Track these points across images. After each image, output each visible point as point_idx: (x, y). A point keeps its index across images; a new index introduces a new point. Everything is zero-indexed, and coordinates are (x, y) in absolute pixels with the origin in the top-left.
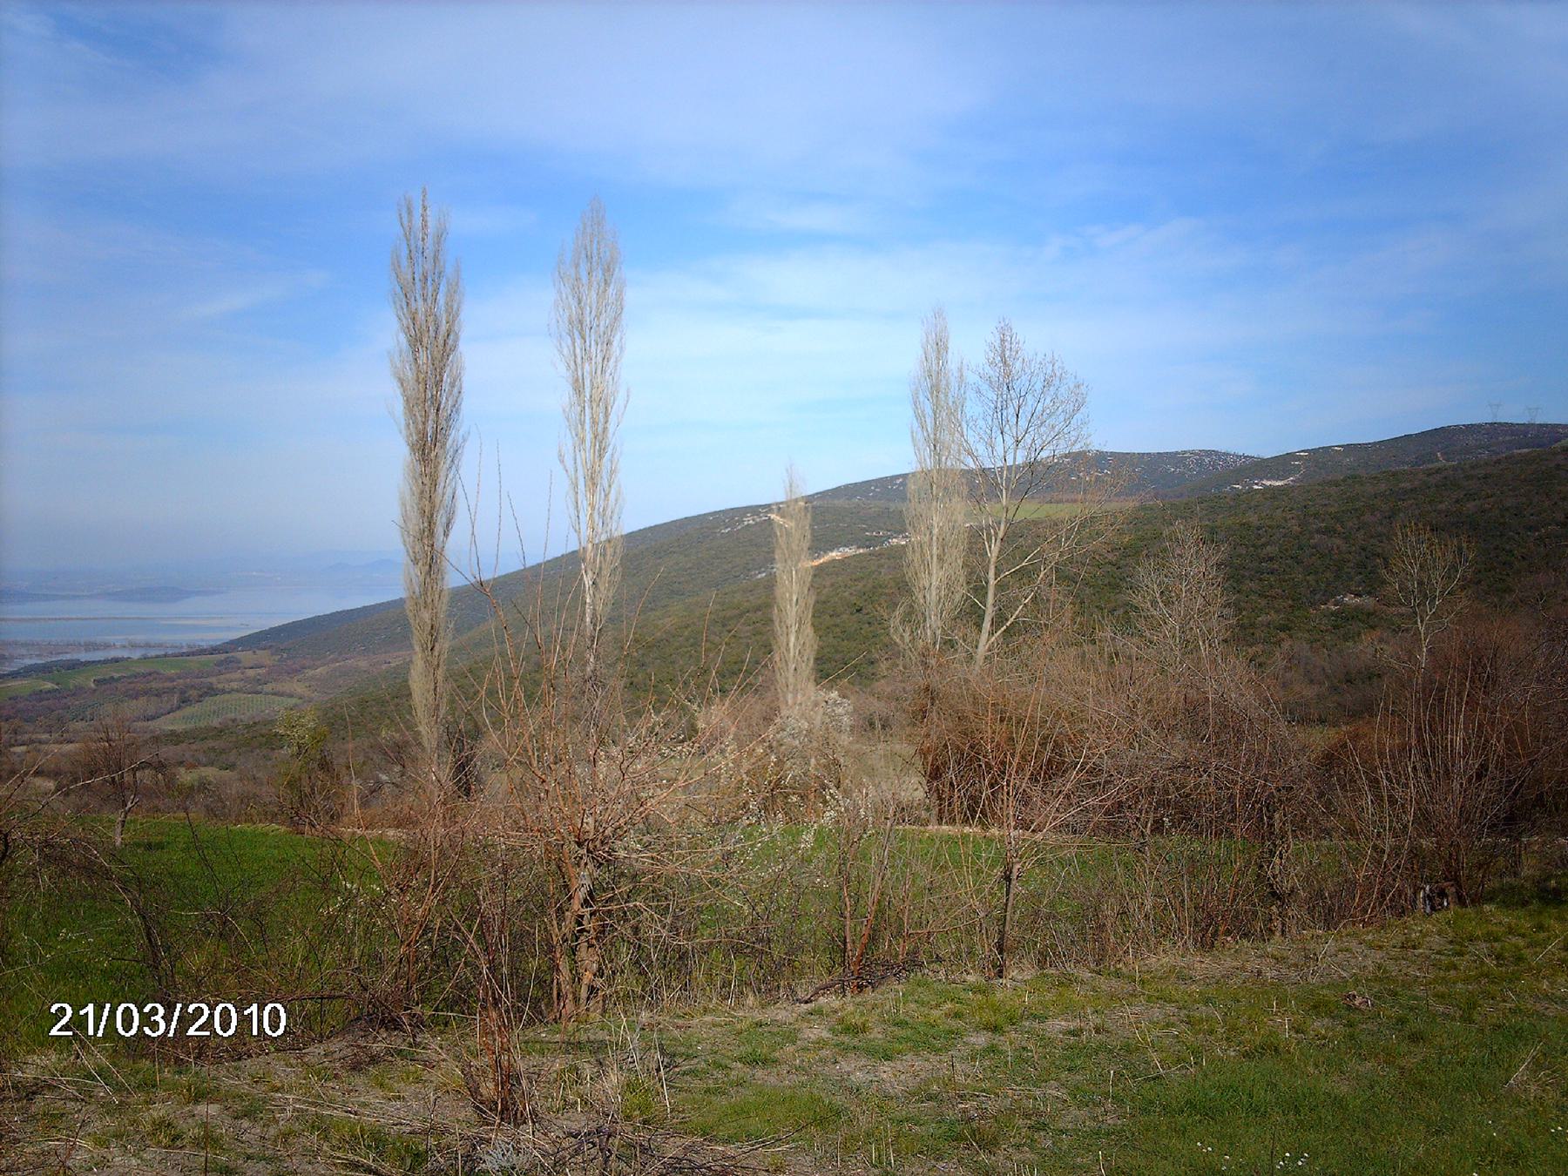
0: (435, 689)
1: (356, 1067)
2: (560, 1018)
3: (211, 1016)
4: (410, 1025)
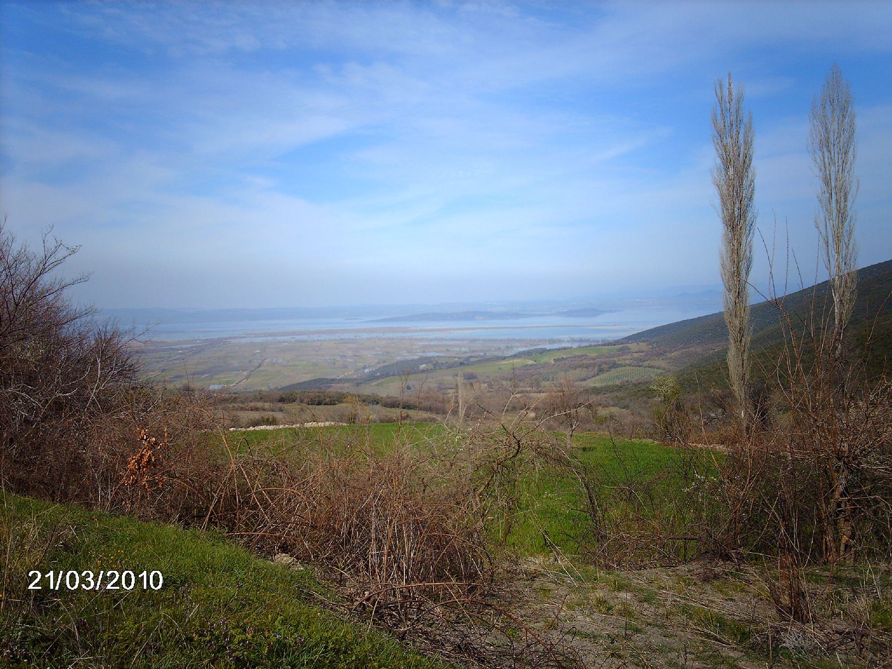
0: (743, 365)
1: (706, 580)
2: (827, 562)
3: (120, 578)
4: (737, 559)
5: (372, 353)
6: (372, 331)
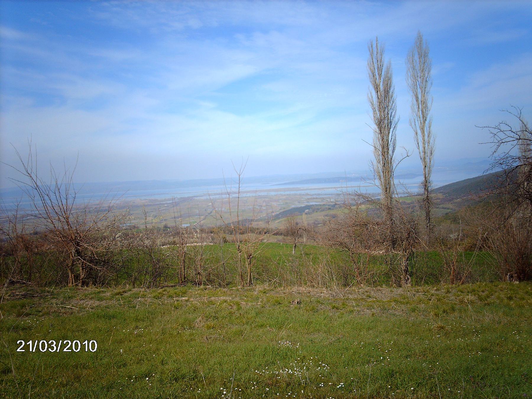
3: (72, 345)
5: (277, 204)
6: (285, 190)
